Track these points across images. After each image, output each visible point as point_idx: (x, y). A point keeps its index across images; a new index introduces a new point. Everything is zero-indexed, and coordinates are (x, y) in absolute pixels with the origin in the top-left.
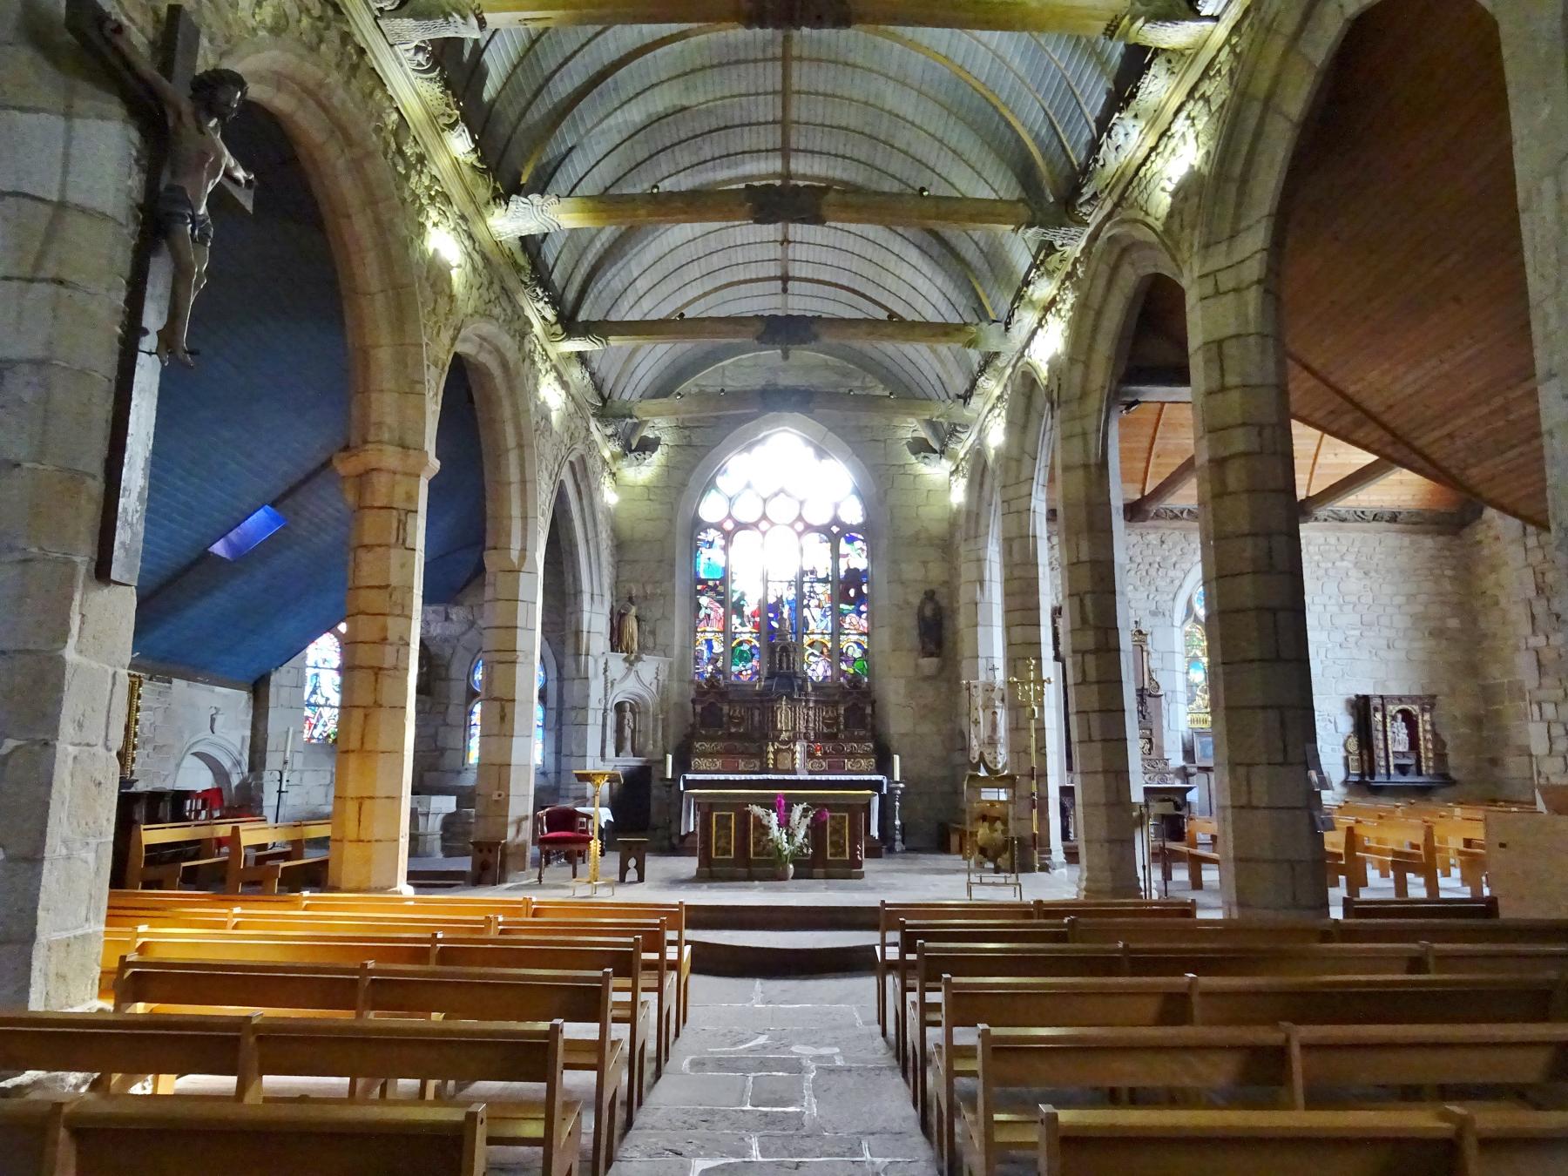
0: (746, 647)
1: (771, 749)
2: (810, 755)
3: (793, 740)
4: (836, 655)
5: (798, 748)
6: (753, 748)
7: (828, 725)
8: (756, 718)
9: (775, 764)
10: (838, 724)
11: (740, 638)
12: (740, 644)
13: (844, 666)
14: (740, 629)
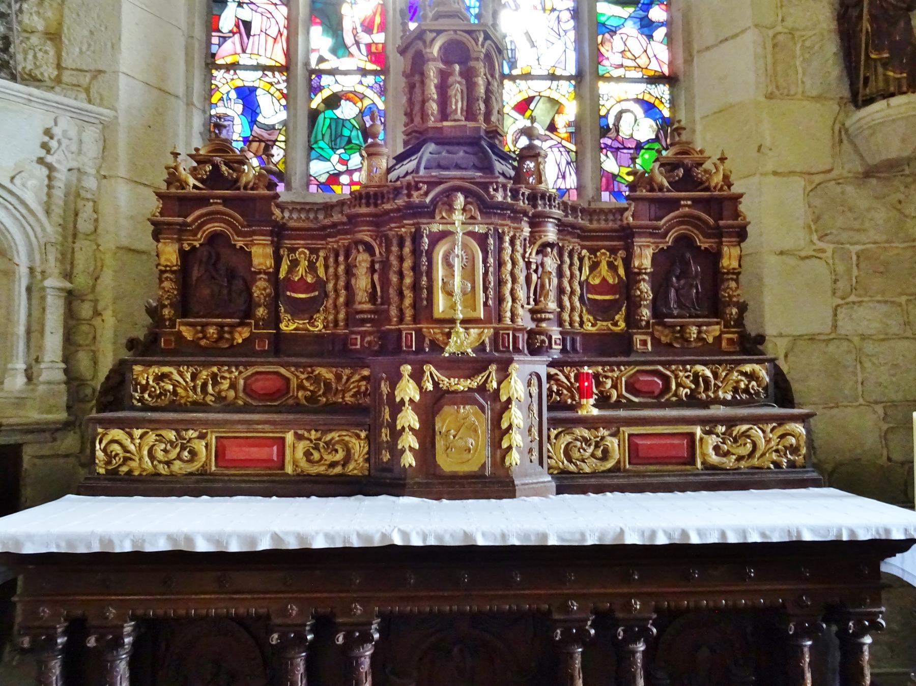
0: (347, 111)
1: (408, 390)
2: (558, 412)
3: (496, 356)
4: (594, 132)
5: (517, 386)
6: (352, 383)
7: (602, 311)
8: (362, 283)
9: (427, 451)
10: (633, 305)
11: (330, 85)
12: (333, 102)
13: (610, 164)
14: (333, 62)
